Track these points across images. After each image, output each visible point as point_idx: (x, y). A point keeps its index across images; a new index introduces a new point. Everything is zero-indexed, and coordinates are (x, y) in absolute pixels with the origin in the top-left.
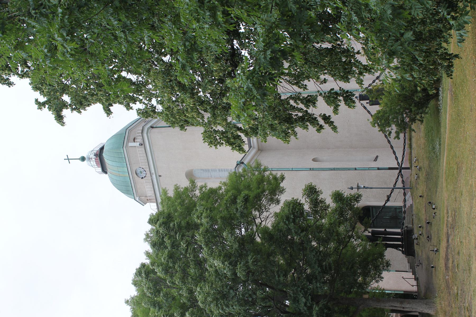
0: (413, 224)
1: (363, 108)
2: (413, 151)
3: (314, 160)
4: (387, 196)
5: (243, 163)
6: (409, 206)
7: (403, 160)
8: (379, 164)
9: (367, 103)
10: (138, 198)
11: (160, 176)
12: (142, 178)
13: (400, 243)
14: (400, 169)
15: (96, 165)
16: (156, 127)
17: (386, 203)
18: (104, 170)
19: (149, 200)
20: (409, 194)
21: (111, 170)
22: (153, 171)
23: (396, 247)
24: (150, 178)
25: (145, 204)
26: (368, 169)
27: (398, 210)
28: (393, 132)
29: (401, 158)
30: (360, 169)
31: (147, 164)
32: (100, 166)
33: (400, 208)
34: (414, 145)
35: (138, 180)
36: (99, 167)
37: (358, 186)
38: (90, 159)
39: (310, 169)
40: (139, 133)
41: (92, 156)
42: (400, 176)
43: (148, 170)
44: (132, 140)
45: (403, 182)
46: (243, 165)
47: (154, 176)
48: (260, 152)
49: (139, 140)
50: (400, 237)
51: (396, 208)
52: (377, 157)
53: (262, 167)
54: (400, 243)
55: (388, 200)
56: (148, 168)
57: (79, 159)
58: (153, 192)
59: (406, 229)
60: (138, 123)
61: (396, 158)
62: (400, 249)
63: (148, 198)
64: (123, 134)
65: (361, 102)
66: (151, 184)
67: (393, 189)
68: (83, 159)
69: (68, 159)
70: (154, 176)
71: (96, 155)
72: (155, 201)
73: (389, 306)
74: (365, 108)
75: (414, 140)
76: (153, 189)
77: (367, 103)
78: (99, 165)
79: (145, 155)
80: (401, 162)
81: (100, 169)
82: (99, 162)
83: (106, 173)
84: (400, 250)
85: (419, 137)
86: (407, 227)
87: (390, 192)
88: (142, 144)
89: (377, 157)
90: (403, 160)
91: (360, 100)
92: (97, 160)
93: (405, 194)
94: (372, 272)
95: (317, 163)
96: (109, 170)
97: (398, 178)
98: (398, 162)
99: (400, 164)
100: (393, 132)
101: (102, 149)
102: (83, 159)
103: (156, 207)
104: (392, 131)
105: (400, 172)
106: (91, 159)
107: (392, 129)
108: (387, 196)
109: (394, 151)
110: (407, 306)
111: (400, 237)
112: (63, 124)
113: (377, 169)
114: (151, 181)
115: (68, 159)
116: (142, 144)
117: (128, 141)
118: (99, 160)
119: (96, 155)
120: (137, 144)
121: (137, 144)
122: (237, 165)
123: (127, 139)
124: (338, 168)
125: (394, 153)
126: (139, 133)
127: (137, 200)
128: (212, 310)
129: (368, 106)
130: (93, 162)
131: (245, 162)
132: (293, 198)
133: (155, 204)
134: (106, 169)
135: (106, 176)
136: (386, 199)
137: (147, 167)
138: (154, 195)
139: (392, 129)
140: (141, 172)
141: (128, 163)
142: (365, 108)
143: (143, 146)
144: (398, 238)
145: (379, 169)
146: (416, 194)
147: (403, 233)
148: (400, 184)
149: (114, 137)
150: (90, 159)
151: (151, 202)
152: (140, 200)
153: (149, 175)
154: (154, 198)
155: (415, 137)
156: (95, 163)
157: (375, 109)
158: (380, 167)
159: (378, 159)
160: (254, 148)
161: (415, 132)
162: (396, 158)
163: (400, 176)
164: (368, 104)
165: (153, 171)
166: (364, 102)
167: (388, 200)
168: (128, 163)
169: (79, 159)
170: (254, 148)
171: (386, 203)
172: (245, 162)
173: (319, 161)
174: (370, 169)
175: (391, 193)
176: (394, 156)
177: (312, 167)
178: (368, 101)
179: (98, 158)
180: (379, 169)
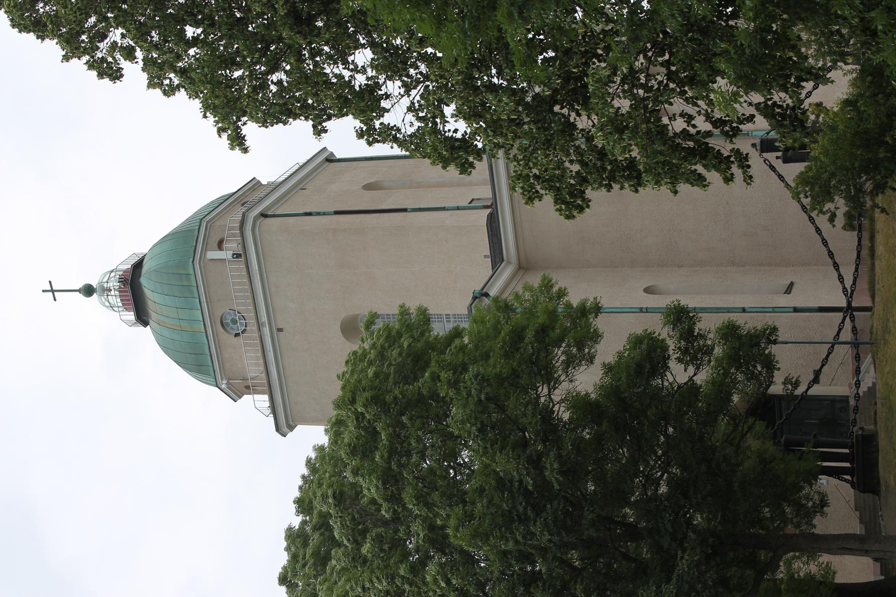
0: (876, 423)
2: (877, 263)
3: (648, 290)
4: (814, 371)
5: (487, 295)
6: (864, 392)
8: (796, 300)
9: (777, 158)
10: (225, 382)
11: (280, 330)
12: (237, 335)
13: (847, 465)
15: (120, 304)
16: (274, 216)
17: (809, 388)
18: (142, 318)
19: (249, 389)
20: (867, 362)
21: (160, 317)
22: (264, 318)
24: (256, 335)
25: (240, 397)
26: (771, 310)
28: (840, 214)
29: (852, 278)
30: (755, 310)
31: (250, 301)
32: (132, 306)
33: (845, 399)
34: (880, 249)
35: (227, 339)
36: (127, 310)
38: (106, 291)
39: (641, 310)
41: (114, 284)
42: (848, 319)
43: (253, 314)
44: (216, 246)
45: (854, 330)
47: (266, 330)
48: (521, 272)
49: (232, 246)
50: (847, 451)
52: (792, 284)
53: (555, 289)
54: (847, 465)
55: (816, 380)
56: (253, 311)
57: (79, 291)
58: (262, 368)
59: (860, 432)
60: (235, 201)
61: (841, 278)
62: (848, 477)
63: (250, 383)
64: (192, 231)
65: (765, 155)
66: (259, 348)
67: (833, 347)
68: (88, 291)
69: (53, 291)
70: (266, 330)
72: (266, 388)
74: (772, 168)
75: (879, 238)
76: (261, 361)
77: (777, 158)
78: (129, 304)
79: (246, 280)
80: (851, 287)
81: (131, 316)
82: (130, 297)
83: (145, 323)
84: (845, 480)
85: (891, 231)
87: (820, 365)
88: (238, 256)
89: (792, 284)
91: (763, 150)
92: (126, 292)
93: (857, 358)
95: (656, 296)
96: (153, 316)
97: (843, 322)
98: (844, 288)
99: (849, 291)
100: (840, 214)
101: (138, 266)
102: (88, 291)
103: (268, 404)
104: (837, 213)
105: (849, 303)
106: (110, 290)
107: (837, 208)
108: (814, 371)
110: (874, 548)
111: (847, 451)
112: (245, 150)
113: (791, 310)
114: (258, 342)
115: (53, 291)
116: (238, 256)
117: (205, 249)
118: (129, 294)
120: (226, 255)
121: (226, 255)
122: (475, 298)
123: (203, 244)
124: (705, 308)
125: (836, 266)
127: (223, 386)
129: (779, 165)
130: (116, 300)
132: (646, 330)
133: (266, 397)
136: (812, 377)
137: (251, 308)
138: (264, 375)
139: (837, 208)
140: (234, 322)
141: (204, 300)
142: (772, 168)
143: (243, 259)
146: (883, 355)
147: (853, 444)
148: (846, 335)
149: (168, 238)
150: (106, 291)
152: (228, 388)
153: (255, 328)
154: (265, 381)
155: (883, 230)
156: (119, 300)
157: (793, 170)
158: (799, 305)
159: (794, 290)
160: (509, 262)
161: (888, 214)
162: (841, 278)
163: (848, 319)
165: (264, 318)
166: (771, 156)
167: (816, 380)
168: (204, 300)
169: (79, 291)
171: (809, 388)
172: (493, 292)
173: (660, 294)
174: (776, 310)
175: (829, 354)
176: (836, 274)
177: (644, 306)
179: (129, 289)
180: (796, 310)
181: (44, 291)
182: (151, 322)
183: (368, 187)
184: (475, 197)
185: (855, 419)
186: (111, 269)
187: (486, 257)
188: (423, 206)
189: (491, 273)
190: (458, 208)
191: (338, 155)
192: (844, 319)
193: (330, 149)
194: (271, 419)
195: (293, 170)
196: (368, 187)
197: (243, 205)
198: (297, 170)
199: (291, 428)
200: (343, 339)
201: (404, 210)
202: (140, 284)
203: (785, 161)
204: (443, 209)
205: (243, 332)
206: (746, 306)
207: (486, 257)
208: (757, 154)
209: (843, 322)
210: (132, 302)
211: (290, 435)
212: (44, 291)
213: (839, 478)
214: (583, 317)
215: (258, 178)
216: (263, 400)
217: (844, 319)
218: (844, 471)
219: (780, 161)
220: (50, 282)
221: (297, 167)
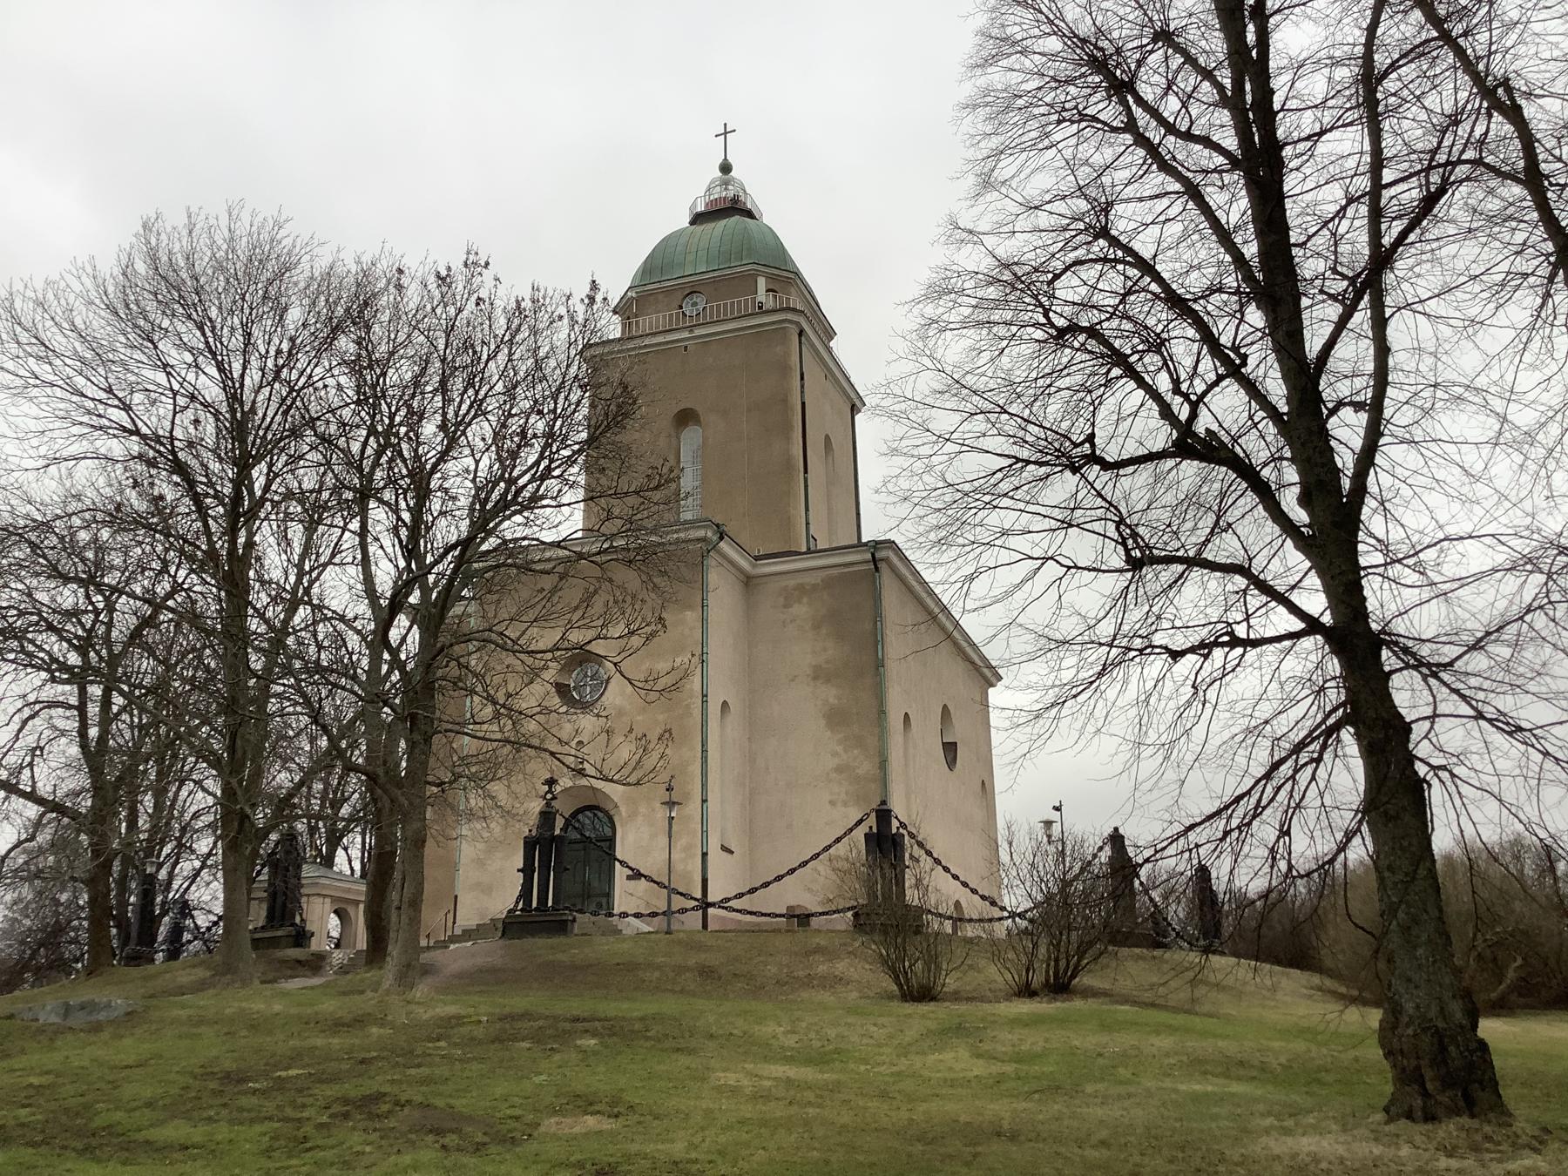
3: (725, 704)
5: (721, 538)
7: (734, 910)
9: (871, 828)
13: (534, 904)
14: (705, 905)
18: (697, 219)
19: (626, 326)
23: (526, 893)
27: (604, 901)
33: (610, 906)
37: (674, 803)
38: (726, 184)
40: (787, 303)
46: (715, 538)
50: (550, 904)
51: (609, 895)
54: (534, 904)
62: (520, 906)
65: (873, 815)
68: (726, 168)
69: (725, 133)
71: (735, 199)
73: (1197, 1065)
77: (871, 828)
81: (700, 208)
83: (692, 223)
84: (517, 903)
86: (574, 920)
90: (734, 910)
94: (955, 349)
96: (698, 228)
98: (729, 899)
101: (749, 214)
102: (726, 168)
109: (757, 889)
111: (550, 904)
115: (725, 133)
116: (760, 308)
119: (735, 199)
122: (718, 525)
126: (787, 303)
128: (422, 1069)
131: (722, 544)
133: (618, 335)
134: (701, 223)
135: (685, 221)
145: (705, 855)
150: (726, 184)
151: (624, 326)
164: (867, 830)
166: (872, 821)
170: (754, 566)
178: (875, 830)
180: (705, 855)
218: (528, 901)
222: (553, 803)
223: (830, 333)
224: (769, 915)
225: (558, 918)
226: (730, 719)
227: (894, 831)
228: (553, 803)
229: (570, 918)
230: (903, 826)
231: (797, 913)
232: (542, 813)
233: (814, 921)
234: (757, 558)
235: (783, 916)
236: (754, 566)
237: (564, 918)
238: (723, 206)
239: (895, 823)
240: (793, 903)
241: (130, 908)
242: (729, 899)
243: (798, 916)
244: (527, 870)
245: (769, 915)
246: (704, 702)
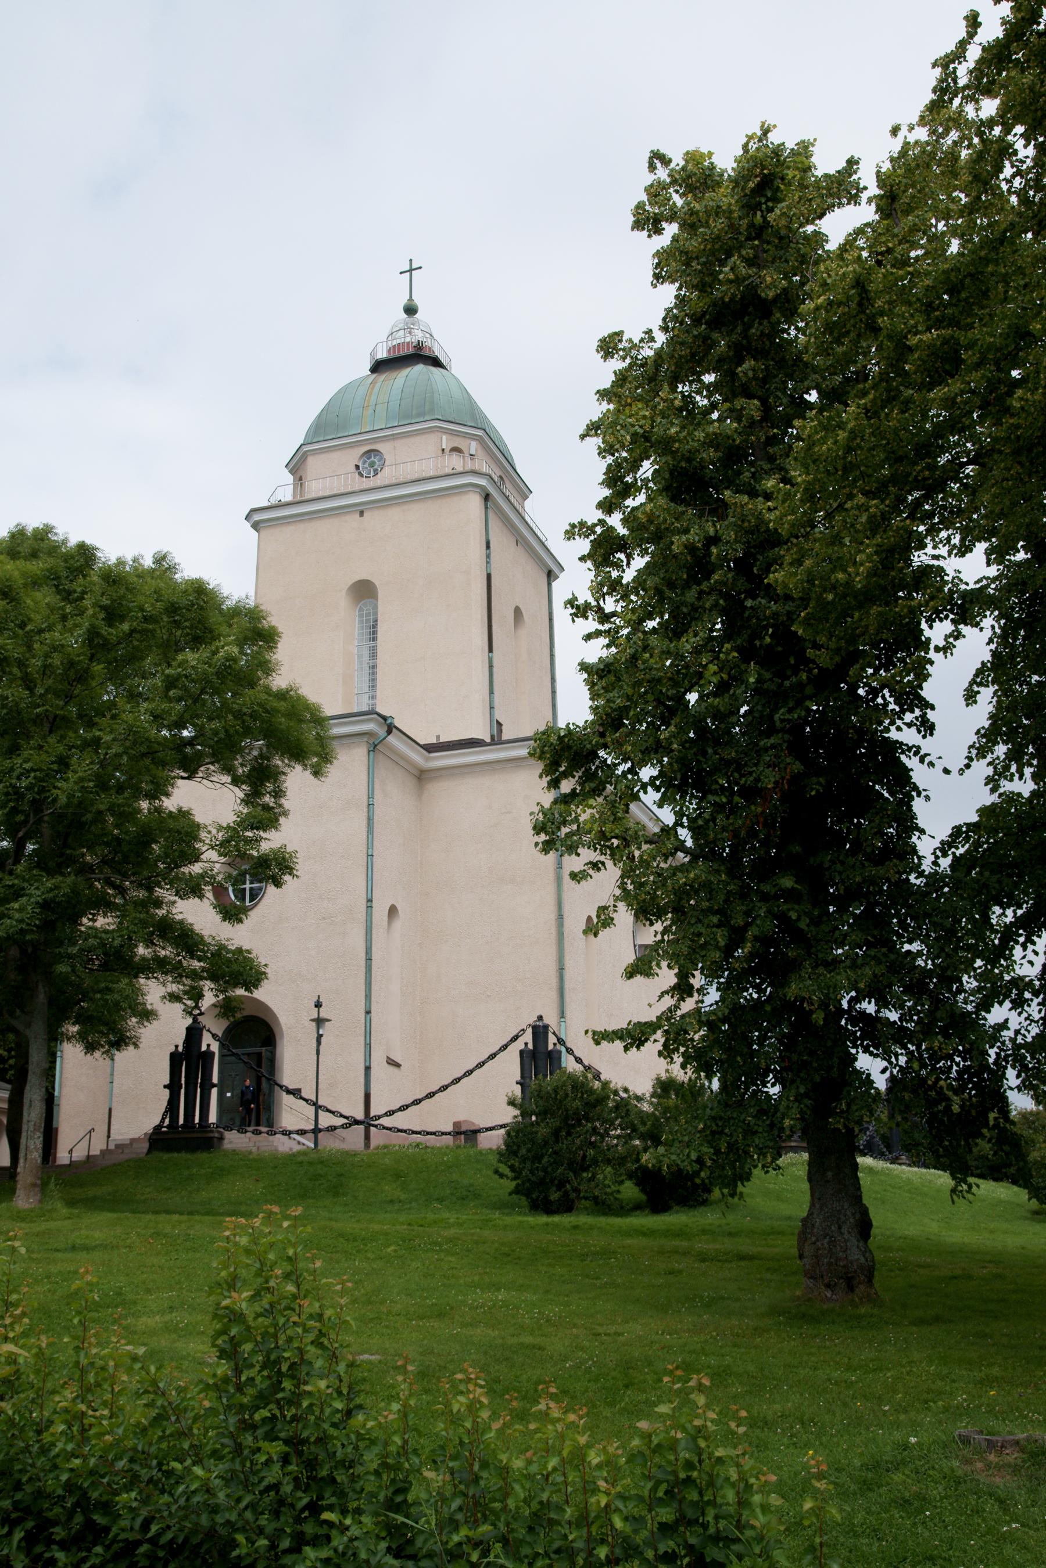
1: (515, 1033)
3: (393, 911)
5: (389, 732)
9: (526, 1044)
11: (362, 513)
12: (357, 467)
13: (181, 1121)
18: (378, 367)
19: (299, 480)
33: (270, 1124)
35: (353, 456)
36: (389, 351)
41: (418, 336)
42: (345, 1121)
50: (197, 1120)
52: (398, 1065)
54: (181, 1121)
57: (411, 299)
62: (167, 1122)
65: (530, 1031)
67: (320, 1107)
68: (410, 310)
69: (411, 270)
74: (515, 1038)
77: (526, 1044)
78: (394, 352)
81: (382, 354)
89: (398, 1065)
97: (342, 1116)
99: (376, 1123)
101: (436, 362)
102: (410, 310)
111: (197, 1120)
115: (411, 270)
125: (403, 1108)
129: (519, 1045)
130: (400, 338)
137: (387, 482)
142: (515, 1038)
144: (194, 1116)
145: (368, 1069)
148: (326, 1120)
149: (465, 395)
158: (373, 1072)
159: (392, 1069)
162: (390, 1113)
163: (345, 1121)
166: (528, 1037)
169: (411, 299)
170: (427, 759)
172: (391, 739)
178: (530, 1046)
179: (411, 351)
180: (368, 1069)
181: (411, 260)
182: (375, 375)
183: (518, 612)
184: (504, 728)
185: (261, 1133)
186: (434, 334)
187: (438, 737)
188: (495, 670)
189: (422, 743)
190: (492, 708)
191: (554, 584)
192: (375, 1126)
193: (562, 576)
194: (265, 504)
195: (539, 534)
196: (518, 612)
197: (501, 477)
198: (541, 541)
199: (256, 526)
200: (350, 583)
201: (491, 650)
202: (418, 363)
203: (522, 1052)
204: (491, 692)
205: (360, 474)
206: (373, 1014)
207: (438, 737)
208: (531, 1022)
209: (342, 1116)
210: (397, 354)
211: (248, 525)
212: (411, 260)
213: (166, 1112)
214: (19, 553)
215: (531, 496)
216: (286, 495)
217: (375, 1126)
218: (174, 1117)
219: (523, 1047)
220: (420, 268)
221: (544, 540)
222: (200, 1018)
223: (524, 492)
224: (419, 1133)
225: (189, 1136)
226: (398, 924)
227: (551, 1047)
228: (200, 1018)
229: (216, 1135)
230: (561, 1041)
231: (463, 1129)
232: (189, 1029)
233: (481, 1137)
234: (430, 748)
235: (449, 1134)
236: (427, 759)
237: (211, 1135)
238: (401, 353)
239: (552, 1039)
240: (461, 1118)
241: (794, 679)
242: (342, 1126)
243: (464, 1133)
244: (173, 1087)
245: (419, 1133)
246: (369, 907)
